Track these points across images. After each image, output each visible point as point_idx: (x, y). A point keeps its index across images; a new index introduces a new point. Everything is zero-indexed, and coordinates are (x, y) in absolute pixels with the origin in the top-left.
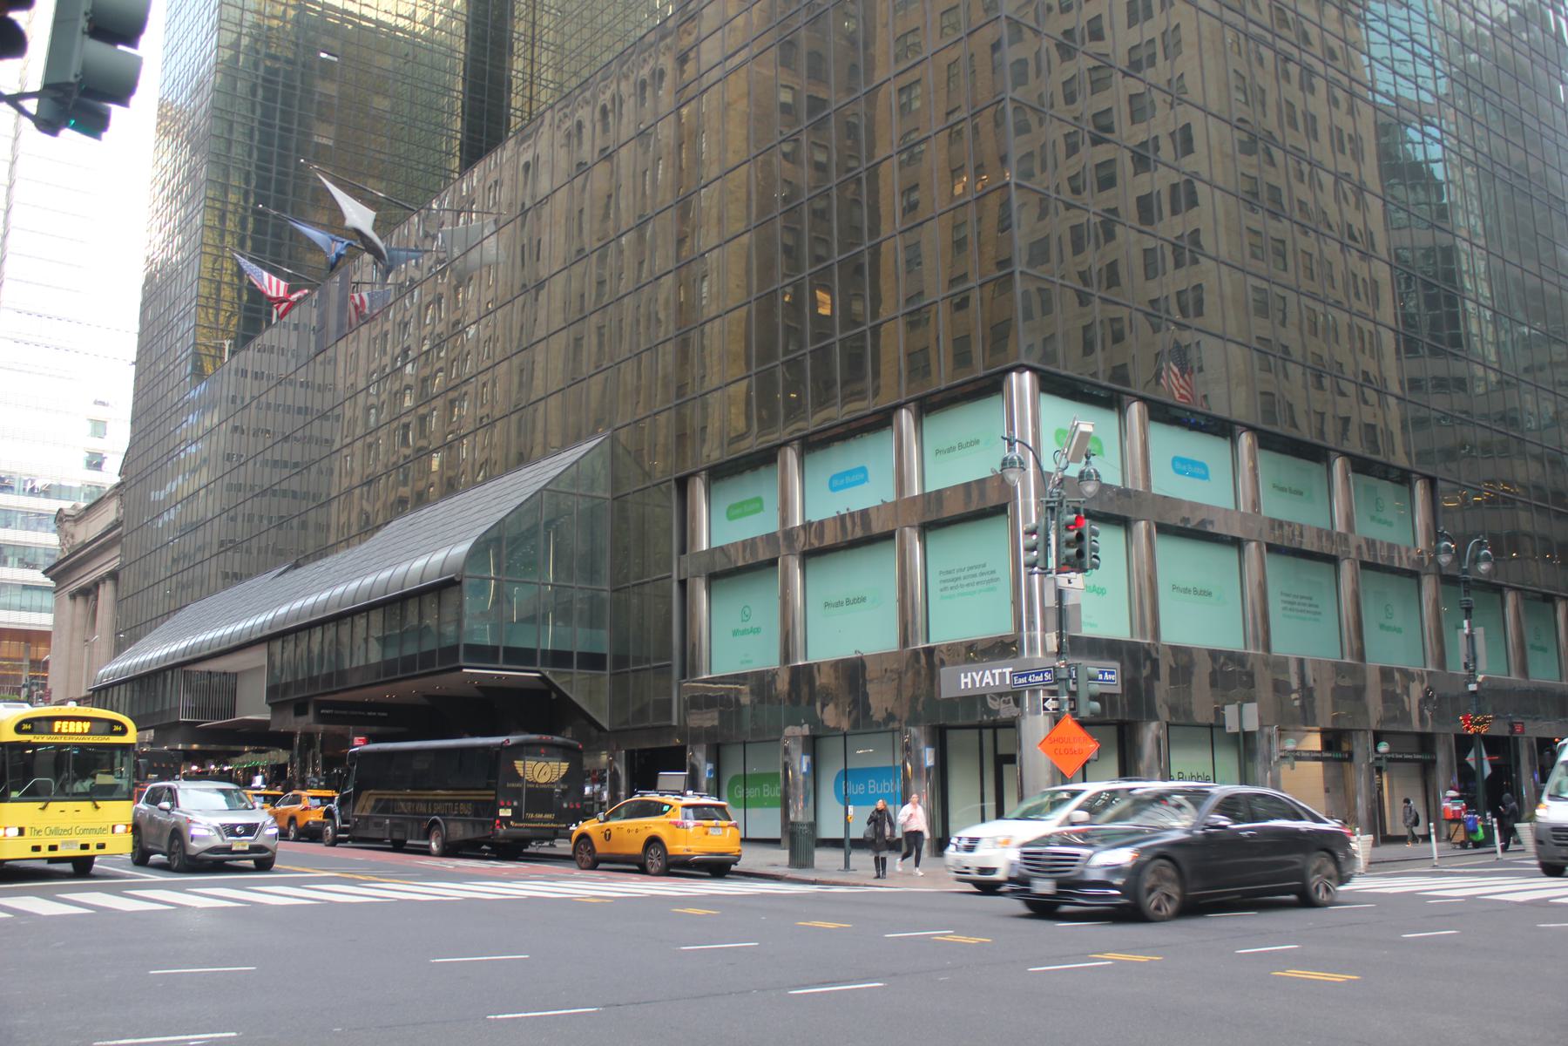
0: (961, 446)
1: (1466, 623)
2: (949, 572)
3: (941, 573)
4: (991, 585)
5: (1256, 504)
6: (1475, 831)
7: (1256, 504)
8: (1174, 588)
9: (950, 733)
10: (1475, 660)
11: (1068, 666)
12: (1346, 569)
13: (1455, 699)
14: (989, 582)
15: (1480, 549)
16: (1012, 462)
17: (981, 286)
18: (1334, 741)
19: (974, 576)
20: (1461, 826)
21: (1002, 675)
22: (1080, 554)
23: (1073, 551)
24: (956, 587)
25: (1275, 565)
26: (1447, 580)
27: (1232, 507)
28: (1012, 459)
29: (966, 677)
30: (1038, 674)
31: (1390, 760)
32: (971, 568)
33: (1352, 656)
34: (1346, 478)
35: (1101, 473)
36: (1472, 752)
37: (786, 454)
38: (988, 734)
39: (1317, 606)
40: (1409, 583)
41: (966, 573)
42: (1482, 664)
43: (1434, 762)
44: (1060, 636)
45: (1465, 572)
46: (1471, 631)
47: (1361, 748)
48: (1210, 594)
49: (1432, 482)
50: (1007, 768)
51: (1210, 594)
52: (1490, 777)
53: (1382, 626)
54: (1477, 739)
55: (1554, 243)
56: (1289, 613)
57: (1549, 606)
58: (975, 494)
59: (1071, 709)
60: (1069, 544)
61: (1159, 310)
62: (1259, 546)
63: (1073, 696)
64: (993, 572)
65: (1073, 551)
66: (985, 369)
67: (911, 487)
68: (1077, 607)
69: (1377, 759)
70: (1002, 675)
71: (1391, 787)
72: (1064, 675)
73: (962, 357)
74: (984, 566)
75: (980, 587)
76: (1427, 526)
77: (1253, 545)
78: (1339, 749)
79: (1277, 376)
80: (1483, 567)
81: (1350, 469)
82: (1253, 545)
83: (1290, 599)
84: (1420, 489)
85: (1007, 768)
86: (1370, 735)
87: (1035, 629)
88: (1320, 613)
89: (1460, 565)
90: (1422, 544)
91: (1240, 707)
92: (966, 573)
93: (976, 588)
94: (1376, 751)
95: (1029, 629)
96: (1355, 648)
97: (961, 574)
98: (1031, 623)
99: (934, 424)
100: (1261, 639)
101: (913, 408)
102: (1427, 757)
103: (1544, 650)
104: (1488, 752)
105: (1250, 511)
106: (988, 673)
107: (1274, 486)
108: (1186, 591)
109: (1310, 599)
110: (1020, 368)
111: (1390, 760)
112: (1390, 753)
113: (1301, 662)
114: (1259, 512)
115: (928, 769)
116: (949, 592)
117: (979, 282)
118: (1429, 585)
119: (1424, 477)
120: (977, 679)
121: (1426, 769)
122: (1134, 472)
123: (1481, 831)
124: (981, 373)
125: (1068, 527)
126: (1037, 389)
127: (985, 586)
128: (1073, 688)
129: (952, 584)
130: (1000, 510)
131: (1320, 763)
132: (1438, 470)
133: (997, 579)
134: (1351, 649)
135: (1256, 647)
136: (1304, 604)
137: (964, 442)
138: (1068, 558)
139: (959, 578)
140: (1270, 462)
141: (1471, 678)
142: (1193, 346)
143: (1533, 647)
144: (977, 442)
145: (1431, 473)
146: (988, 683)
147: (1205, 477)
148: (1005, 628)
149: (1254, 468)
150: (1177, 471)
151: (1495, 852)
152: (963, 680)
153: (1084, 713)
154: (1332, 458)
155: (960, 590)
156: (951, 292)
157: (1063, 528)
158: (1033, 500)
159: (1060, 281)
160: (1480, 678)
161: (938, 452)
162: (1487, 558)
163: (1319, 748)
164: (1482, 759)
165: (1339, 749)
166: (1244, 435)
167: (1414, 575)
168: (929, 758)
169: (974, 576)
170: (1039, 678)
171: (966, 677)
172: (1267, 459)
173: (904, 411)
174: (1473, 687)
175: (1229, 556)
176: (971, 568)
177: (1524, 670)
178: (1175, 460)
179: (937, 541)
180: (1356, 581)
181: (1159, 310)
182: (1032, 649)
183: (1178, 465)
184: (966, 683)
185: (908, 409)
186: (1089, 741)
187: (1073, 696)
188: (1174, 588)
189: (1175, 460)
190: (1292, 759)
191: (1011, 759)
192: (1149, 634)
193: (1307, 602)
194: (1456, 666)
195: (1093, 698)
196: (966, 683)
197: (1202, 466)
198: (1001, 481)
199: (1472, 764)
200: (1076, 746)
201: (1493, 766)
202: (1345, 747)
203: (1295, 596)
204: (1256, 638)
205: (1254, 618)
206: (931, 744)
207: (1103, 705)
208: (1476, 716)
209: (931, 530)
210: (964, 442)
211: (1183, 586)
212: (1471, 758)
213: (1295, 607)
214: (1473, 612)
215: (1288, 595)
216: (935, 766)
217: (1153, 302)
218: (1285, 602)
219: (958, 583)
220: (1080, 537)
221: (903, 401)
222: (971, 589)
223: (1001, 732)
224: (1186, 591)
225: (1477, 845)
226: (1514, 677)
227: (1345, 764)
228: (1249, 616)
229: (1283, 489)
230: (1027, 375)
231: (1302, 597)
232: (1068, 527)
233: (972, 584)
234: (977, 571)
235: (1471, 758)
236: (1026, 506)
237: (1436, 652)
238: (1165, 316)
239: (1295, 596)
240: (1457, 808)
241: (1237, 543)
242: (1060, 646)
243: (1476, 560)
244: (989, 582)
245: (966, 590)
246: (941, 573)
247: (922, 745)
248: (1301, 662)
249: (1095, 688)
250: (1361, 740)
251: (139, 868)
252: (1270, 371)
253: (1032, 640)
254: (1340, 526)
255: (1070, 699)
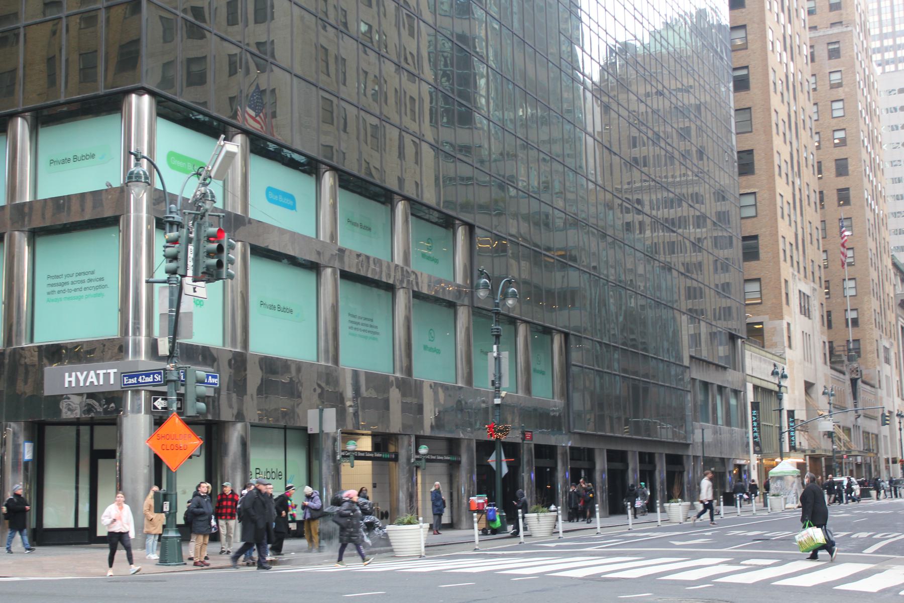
0: (76, 158)
1: (495, 347)
2: (58, 277)
3: (49, 277)
4: (99, 291)
5: (333, 237)
6: (494, 520)
7: (333, 237)
8: (262, 303)
9: (49, 430)
10: (500, 378)
11: (178, 369)
12: (402, 297)
13: (486, 410)
14: (97, 288)
15: (509, 287)
16: (138, 176)
17: (108, 8)
18: (382, 442)
19: (83, 282)
20: (484, 516)
21: (107, 375)
22: (220, 264)
23: (214, 261)
24: (64, 291)
25: (345, 288)
26: (477, 312)
27: (314, 236)
28: (138, 173)
29: (70, 376)
30: (148, 375)
31: (428, 461)
32: (80, 274)
33: (401, 371)
34: (406, 221)
35: (783, 144)
36: (494, 455)
37: (131, 97)
38: (85, 430)
39: (376, 327)
40: (447, 312)
41: (74, 279)
42: (506, 382)
43: (459, 462)
44: (173, 342)
45: (497, 305)
46: (498, 354)
47: (404, 449)
48: (291, 311)
49: (471, 228)
50: (102, 463)
51: (291, 311)
52: (506, 475)
53: (425, 347)
54: (498, 445)
55: (572, 42)
56: (352, 331)
57: (548, 338)
58: (89, 204)
59: (178, 409)
60: (209, 254)
61: (265, 54)
62: (334, 273)
63: (181, 398)
64: (102, 279)
65: (214, 261)
66: (105, 88)
67: (23, 194)
68: (190, 315)
69: (417, 459)
70: (107, 375)
71: (423, 483)
72: (174, 377)
73: (87, 73)
74: (93, 273)
75: (88, 292)
76: (465, 266)
77: (329, 271)
78: (386, 450)
79: (338, 129)
80: (510, 302)
81: (409, 212)
82: (329, 271)
83: (356, 320)
84: (461, 232)
85: (102, 463)
86: (413, 439)
87: (140, 334)
88: (378, 333)
89: (494, 299)
90: (459, 280)
91: (321, 411)
92: (74, 279)
93: (83, 293)
94: (417, 453)
95: (134, 334)
96: (405, 365)
97: (69, 280)
98: (137, 329)
99: (48, 135)
100: (331, 355)
101: (29, 118)
102: (454, 459)
103: (543, 373)
104: (506, 456)
105: (328, 241)
106: (92, 373)
107: (349, 221)
108: (272, 307)
109: (372, 320)
110: (141, 91)
111: (428, 461)
112: (427, 454)
113: (356, 374)
114: (336, 243)
115: (26, 463)
116: (56, 296)
117: (105, 4)
118: (463, 314)
119: (465, 223)
120: (82, 378)
121: (454, 466)
122: (234, 195)
123: (498, 520)
124: (102, 91)
125: (209, 239)
126: (154, 113)
127: (92, 292)
128: (182, 390)
129: (60, 288)
130: (112, 222)
131: (370, 462)
132: (477, 219)
133: (105, 286)
134: (402, 368)
135: (327, 360)
136: (367, 325)
137: (79, 155)
138: (208, 267)
139: (358, 323)
140: (349, 202)
141: (497, 394)
142: (268, 92)
143: (535, 370)
144: (93, 156)
145: (470, 221)
146: (92, 383)
147: (293, 207)
148: (110, 329)
149: (334, 206)
150: (271, 201)
151: (558, 532)
152: (67, 379)
153: (191, 412)
154: (395, 201)
155: (67, 295)
156: (82, 9)
157: (203, 239)
158: (144, 215)
159: (182, 15)
160: (503, 394)
161: (52, 162)
162: (514, 295)
163: (370, 449)
164: (501, 461)
165: (386, 450)
166: (327, 174)
167: (452, 306)
168: (28, 452)
169: (83, 282)
170: (150, 379)
171: (70, 376)
172: (344, 196)
173: (19, 120)
174: (497, 401)
175: (309, 278)
176: (80, 274)
177: (528, 389)
178: (270, 190)
179: (45, 246)
180: (408, 308)
181: (265, 54)
182: (136, 352)
183: (271, 195)
184: (70, 382)
185: (24, 118)
186: (193, 437)
187: (181, 398)
188: (262, 304)
189: (270, 190)
190: (352, 458)
191: (110, 454)
192: (239, 344)
193: (369, 323)
194: (483, 383)
195: (200, 398)
196: (70, 382)
197: (291, 197)
198: (122, 193)
199: (493, 465)
200: (181, 443)
201: (509, 466)
202: (392, 448)
203: (360, 318)
204: (327, 351)
205: (326, 334)
206: (29, 439)
207: (207, 405)
208: (498, 425)
209: (40, 236)
210: (79, 155)
211: (269, 303)
212: (492, 460)
213: (359, 327)
214: (501, 338)
215: (354, 316)
216: (33, 461)
217: (259, 44)
218: (352, 322)
219: (66, 287)
220: (220, 249)
221: (20, 109)
222: (78, 293)
223: (98, 430)
224: (272, 307)
225: (495, 531)
226: (521, 394)
227: (391, 463)
228: (322, 332)
229: (355, 224)
230: (146, 98)
231: (365, 319)
232: (209, 239)
233: (80, 289)
234: (86, 278)
235: (492, 460)
236: (138, 219)
237: (465, 372)
238: (270, 60)
239: (360, 318)
240: (481, 501)
241: (314, 267)
242: (172, 350)
243: (505, 296)
244: (97, 288)
245: (73, 294)
246: (49, 277)
247: (21, 439)
248: (356, 374)
249: (202, 389)
250: (406, 443)
251: (239, 439)
252: (332, 124)
253: (136, 345)
254: (398, 260)
255: (178, 400)
